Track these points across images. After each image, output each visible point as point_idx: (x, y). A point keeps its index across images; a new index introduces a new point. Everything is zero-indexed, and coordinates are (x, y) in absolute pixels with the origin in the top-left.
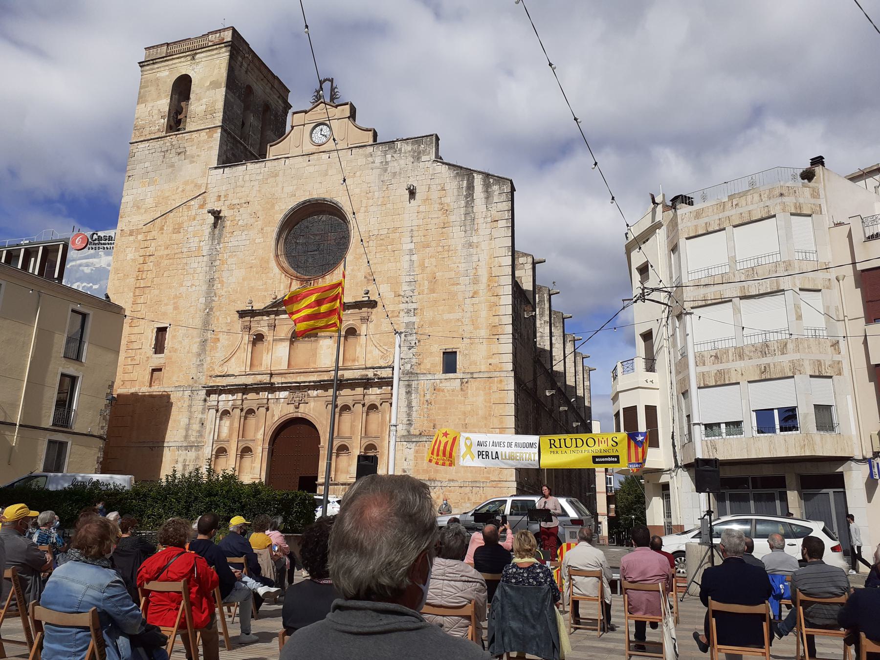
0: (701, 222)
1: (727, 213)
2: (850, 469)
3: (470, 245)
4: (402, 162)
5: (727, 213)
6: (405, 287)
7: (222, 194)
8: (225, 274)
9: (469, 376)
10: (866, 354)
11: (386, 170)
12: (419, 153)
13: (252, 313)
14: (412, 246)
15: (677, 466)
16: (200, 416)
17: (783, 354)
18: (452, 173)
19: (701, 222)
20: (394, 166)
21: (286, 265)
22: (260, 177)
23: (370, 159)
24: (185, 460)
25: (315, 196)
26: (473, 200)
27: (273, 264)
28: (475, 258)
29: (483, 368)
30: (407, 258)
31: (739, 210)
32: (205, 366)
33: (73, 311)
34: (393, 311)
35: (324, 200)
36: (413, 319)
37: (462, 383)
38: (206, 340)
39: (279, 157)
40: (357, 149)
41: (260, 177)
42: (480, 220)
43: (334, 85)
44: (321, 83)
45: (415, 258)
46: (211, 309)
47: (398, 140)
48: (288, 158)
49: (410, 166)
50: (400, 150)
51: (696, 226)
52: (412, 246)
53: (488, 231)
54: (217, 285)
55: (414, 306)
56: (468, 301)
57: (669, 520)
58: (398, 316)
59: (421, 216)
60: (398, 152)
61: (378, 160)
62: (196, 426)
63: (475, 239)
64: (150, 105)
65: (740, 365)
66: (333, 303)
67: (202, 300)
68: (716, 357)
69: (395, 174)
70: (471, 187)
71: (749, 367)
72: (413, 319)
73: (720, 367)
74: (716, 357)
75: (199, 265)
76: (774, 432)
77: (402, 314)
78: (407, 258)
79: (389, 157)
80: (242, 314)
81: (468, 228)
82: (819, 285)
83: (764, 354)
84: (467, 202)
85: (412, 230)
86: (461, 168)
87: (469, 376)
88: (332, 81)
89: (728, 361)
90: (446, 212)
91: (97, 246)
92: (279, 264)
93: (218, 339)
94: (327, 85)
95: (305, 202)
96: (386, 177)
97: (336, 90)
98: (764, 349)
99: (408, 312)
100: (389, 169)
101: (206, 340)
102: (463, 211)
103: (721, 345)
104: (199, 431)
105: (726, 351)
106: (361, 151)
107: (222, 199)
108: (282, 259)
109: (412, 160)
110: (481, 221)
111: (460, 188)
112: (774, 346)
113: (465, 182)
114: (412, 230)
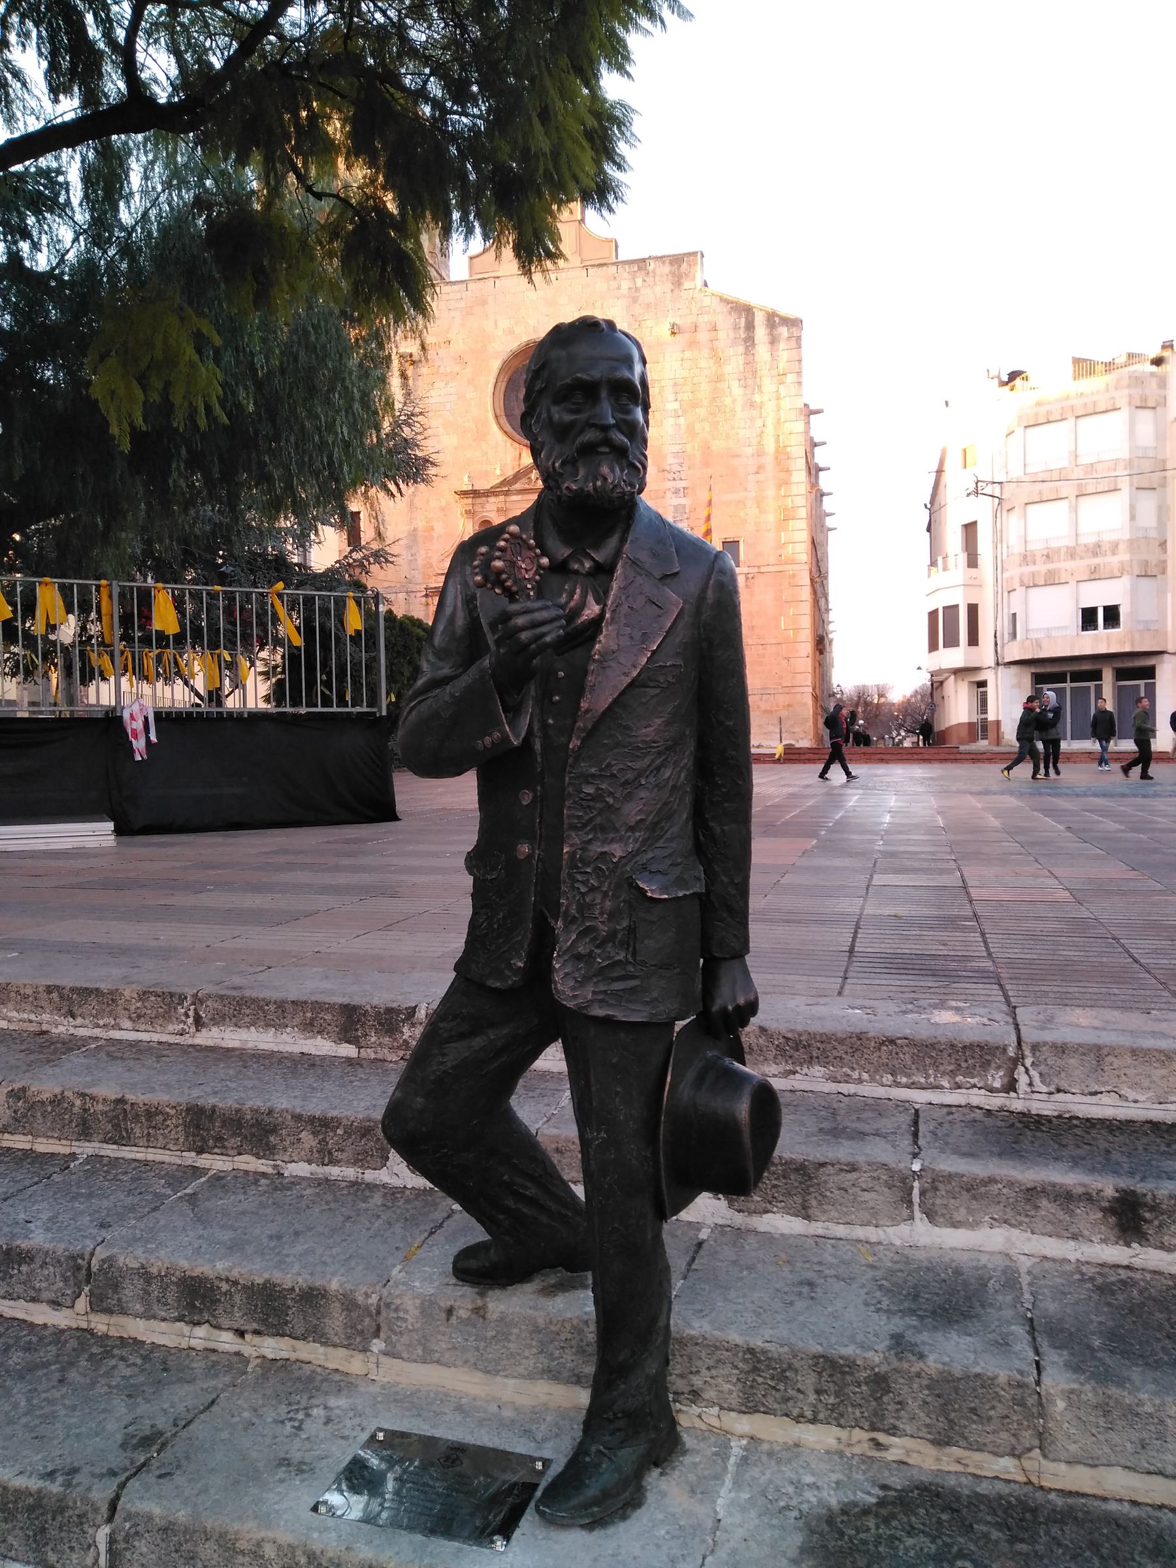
2: (1162, 662)
3: (753, 405)
6: (671, 460)
9: (755, 570)
11: (635, 300)
13: (475, 494)
15: (998, 664)
17: (1114, 554)
21: (508, 428)
22: (462, 304)
23: (614, 284)
26: (753, 345)
27: (495, 428)
28: (759, 423)
29: (772, 560)
30: (671, 421)
34: (657, 491)
36: (683, 501)
37: (747, 579)
39: (486, 276)
40: (595, 269)
41: (462, 304)
42: (764, 371)
45: (682, 420)
47: (650, 258)
49: (669, 295)
50: (654, 272)
52: (676, 405)
53: (773, 388)
55: (683, 484)
56: (751, 478)
57: (984, 716)
58: (663, 497)
59: (687, 364)
60: (651, 274)
61: (625, 285)
63: (757, 398)
65: (1070, 564)
68: (1048, 556)
69: (648, 305)
70: (750, 326)
71: (1080, 566)
72: (683, 501)
73: (1051, 566)
74: (1048, 556)
76: (1096, 628)
77: (669, 494)
78: (671, 421)
80: (464, 494)
81: (750, 382)
82: (456, 945)
83: (1095, 554)
84: (747, 347)
87: (755, 570)
89: (1059, 561)
90: (718, 360)
92: (499, 424)
96: (637, 310)
98: (1096, 550)
99: (676, 492)
100: (641, 298)
102: (741, 360)
103: (1054, 544)
105: (1058, 550)
106: (600, 271)
108: (503, 420)
109: (672, 287)
110: (765, 372)
111: (736, 328)
112: (1106, 547)
113: (743, 320)
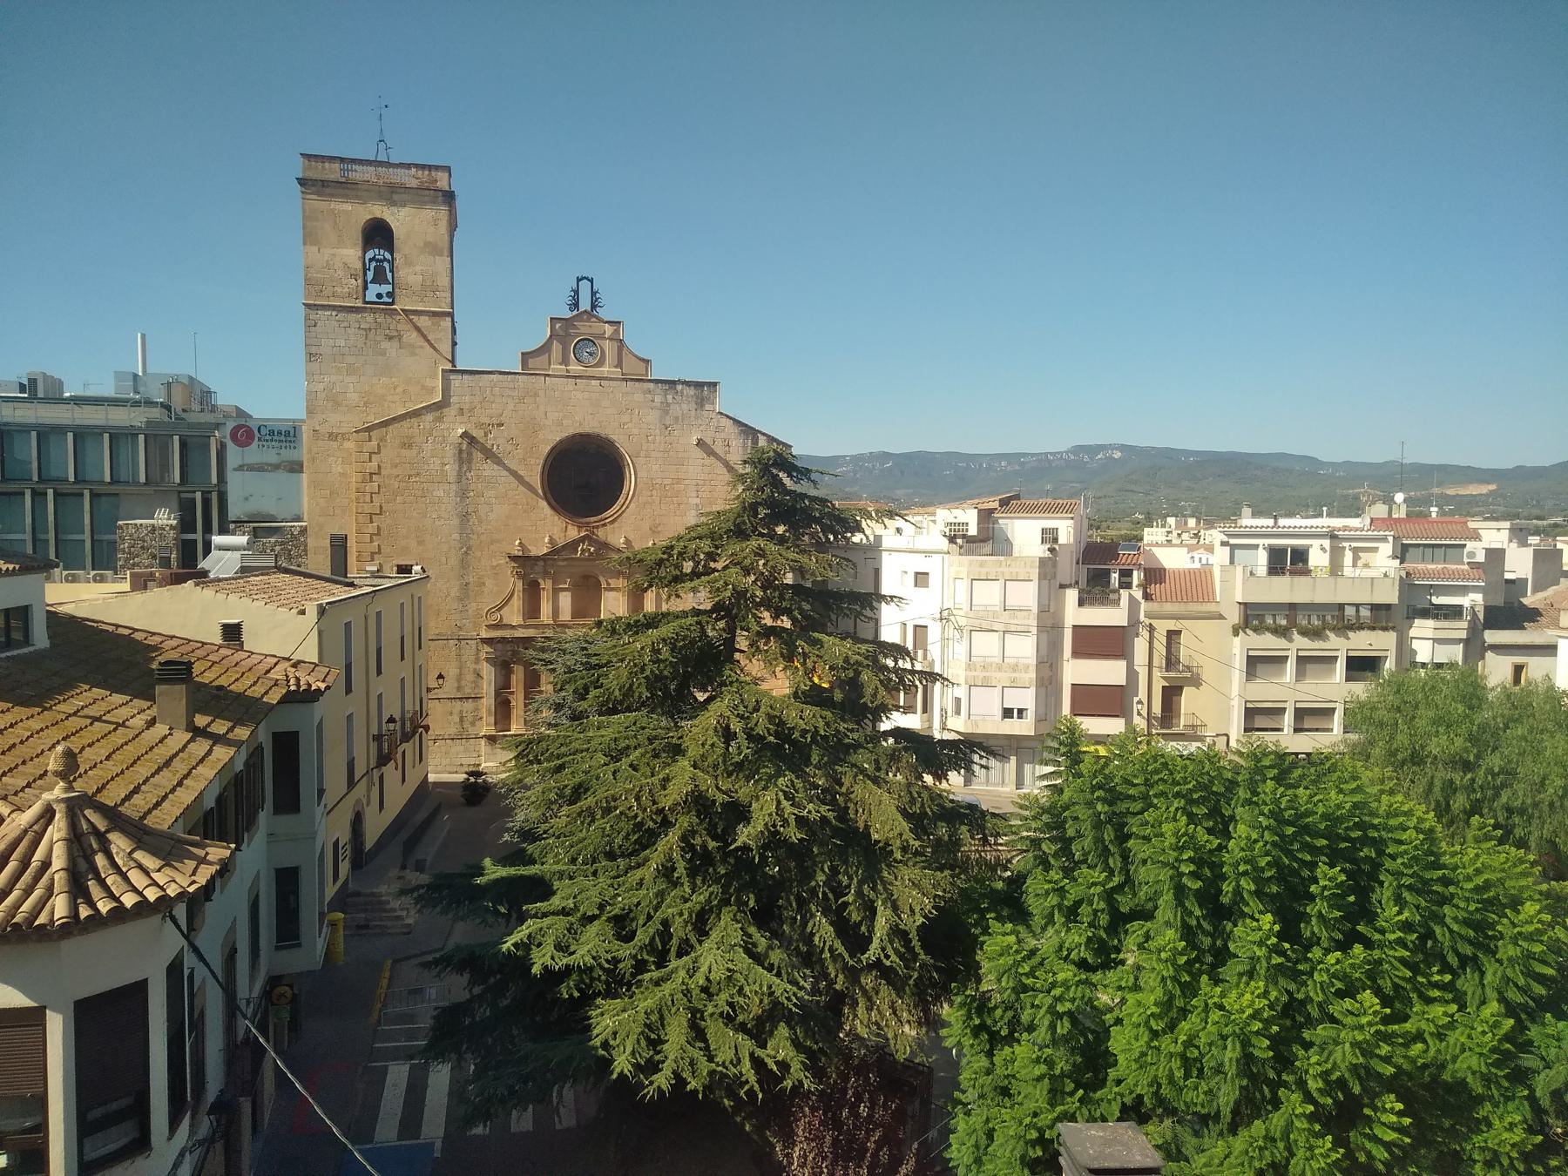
0: (984, 570)
1: (1001, 569)
4: (684, 406)
5: (1001, 569)
7: (466, 407)
8: (482, 510)
10: (1143, 1174)
11: (667, 412)
12: (703, 399)
14: (698, 501)
16: (474, 666)
18: (736, 430)
19: (984, 570)
20: (676, 410)
24: (461, 712)
25: (586, 429)
31: (1011, 570)
32: (470, 612)
33: (402, 604)
35: (598, 436)
38: (467, 584)
43: (595, 288)
44: (579, 280)
46: (469, 548)
48: (548, 375)
49: (693, 413)
51: (980, 572)
52: (698, 501)
54: (473, 519)
61: (658, 399)
62: (470, 677)
64: (327, 251)
65: (998, 675)
66: (540, 491)
67: (456, 536)
69: (677, 418)
75: (445, 493)
79: (670, 397)
85: (697, 485)
86: (746, 425)
88: (591, 281)
91: (284, 444)
93: (484, 584)
94: (585, 287)
95: (574, 436)
97: (598, 295)
101: (467, 584)
103: (988, 660)
104: (474, 682)
107: (467, 414)
114: (697, 485)
